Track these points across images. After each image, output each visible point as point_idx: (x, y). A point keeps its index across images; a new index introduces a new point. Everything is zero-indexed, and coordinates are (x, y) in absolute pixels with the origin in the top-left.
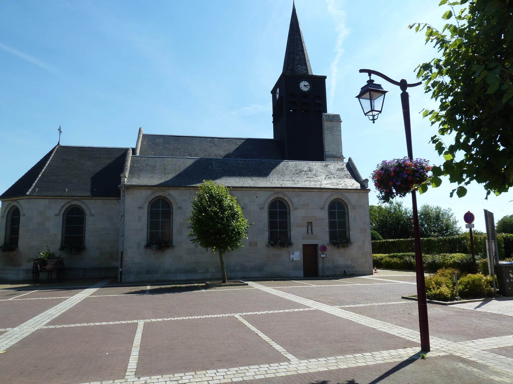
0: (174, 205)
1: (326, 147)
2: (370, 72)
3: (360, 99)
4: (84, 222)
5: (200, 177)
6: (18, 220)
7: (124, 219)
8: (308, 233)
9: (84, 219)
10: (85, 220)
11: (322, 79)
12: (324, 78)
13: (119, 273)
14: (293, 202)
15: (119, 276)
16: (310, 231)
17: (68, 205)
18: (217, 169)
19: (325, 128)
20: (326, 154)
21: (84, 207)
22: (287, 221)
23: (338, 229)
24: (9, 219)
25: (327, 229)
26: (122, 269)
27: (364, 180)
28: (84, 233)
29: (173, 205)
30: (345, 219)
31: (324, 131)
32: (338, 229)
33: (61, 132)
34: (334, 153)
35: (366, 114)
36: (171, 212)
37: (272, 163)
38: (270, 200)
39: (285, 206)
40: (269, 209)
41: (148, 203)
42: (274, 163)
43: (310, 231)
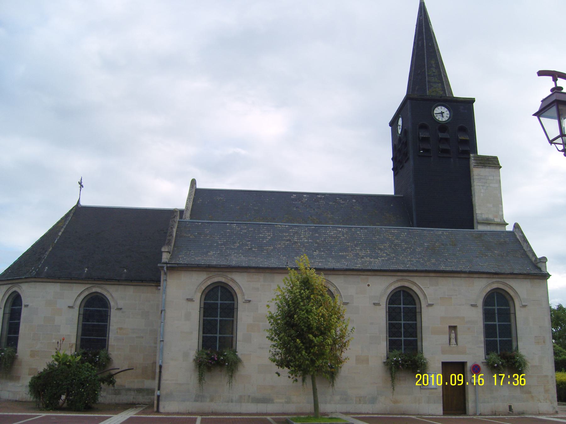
0: (239, 296)
1: (477, 208)
2: (555, 75)
3: (541, 119)
4: (109, 318)
5: (280, 254)
6: (19, 313)
7: (165, 315)
8: (450, 345)
9: (109, 314)
10: (110, 316)
11: (470, 102)
12: (472, 101)
13: (156, 397)
14: (427, 294)
15: (156, 402)
16: (453, 341)
17: (86, 293)
18: (305, 241)
19: (475, 177)
20: (478, 218)
21: (105, 293)
22: (416, 324)
23: (499, 337)
24: (8, 311)
25: (482, 338)
26: (160, 392)
27: (540, 259)
28: (107, 335)
29: (238, 295)
30: (510, 321)
31: (474, 182)
32: (499, 337)
33: (82, 186)
34: (491, 217)
35: (551, 142)
36: (235, 307)
37: (393, 231)
38: (389, 291)
39: (414, 300)
40: (387, 304)
41: (201, 293)
42: (396, 231)
43: (453, 341)
